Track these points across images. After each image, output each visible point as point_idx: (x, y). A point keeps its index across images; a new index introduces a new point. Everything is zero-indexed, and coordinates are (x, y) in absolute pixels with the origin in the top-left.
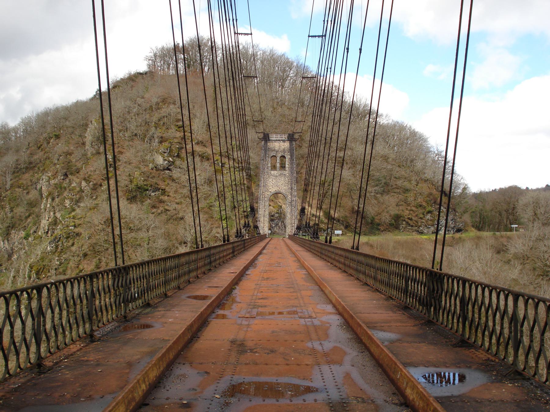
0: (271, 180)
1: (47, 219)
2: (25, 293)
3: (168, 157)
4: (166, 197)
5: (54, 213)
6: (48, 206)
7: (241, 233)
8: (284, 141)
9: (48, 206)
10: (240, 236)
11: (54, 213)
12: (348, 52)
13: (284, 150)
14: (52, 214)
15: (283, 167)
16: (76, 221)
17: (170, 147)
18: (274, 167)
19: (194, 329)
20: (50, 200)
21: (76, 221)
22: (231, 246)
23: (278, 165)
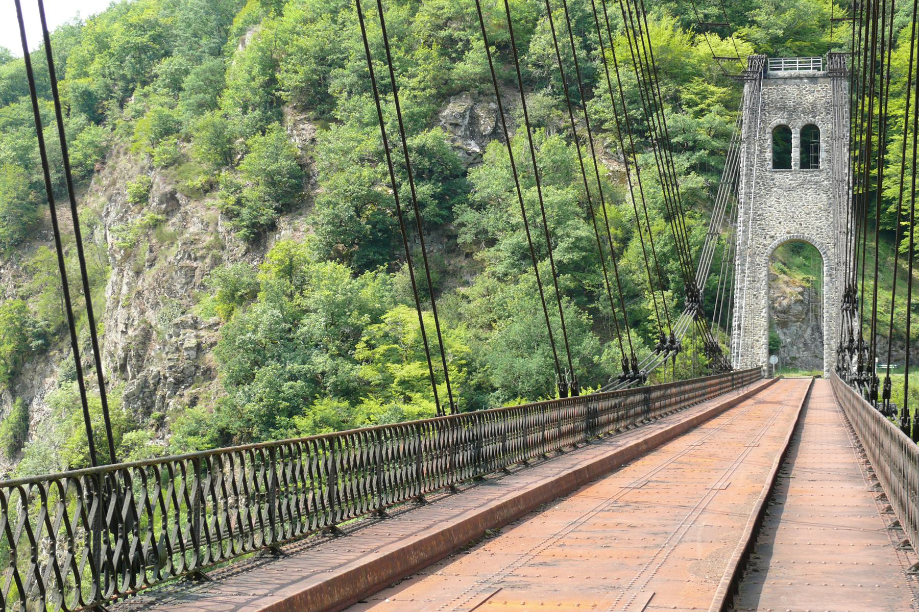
0: (772, 200)
1: (121, 327)
2: (36, 486)
3: (464, 138)
4: (462, 258)
5: (142, 312)
6: (125, 289)
7: (635, 368)
8: (813, 79)
9: (125, 289)
10: (632, 379)
11: (142, 312)
12: (7, 528)
13: (814, 105)
14: (135, 312)
15: (810, 160)
16: (202, 333)
17: (472, 108)
18: (781, 161)
19: (362, 585)
20: (129, 273)
21: (202, 333)
22: (579, 409)
23: (796, 154)
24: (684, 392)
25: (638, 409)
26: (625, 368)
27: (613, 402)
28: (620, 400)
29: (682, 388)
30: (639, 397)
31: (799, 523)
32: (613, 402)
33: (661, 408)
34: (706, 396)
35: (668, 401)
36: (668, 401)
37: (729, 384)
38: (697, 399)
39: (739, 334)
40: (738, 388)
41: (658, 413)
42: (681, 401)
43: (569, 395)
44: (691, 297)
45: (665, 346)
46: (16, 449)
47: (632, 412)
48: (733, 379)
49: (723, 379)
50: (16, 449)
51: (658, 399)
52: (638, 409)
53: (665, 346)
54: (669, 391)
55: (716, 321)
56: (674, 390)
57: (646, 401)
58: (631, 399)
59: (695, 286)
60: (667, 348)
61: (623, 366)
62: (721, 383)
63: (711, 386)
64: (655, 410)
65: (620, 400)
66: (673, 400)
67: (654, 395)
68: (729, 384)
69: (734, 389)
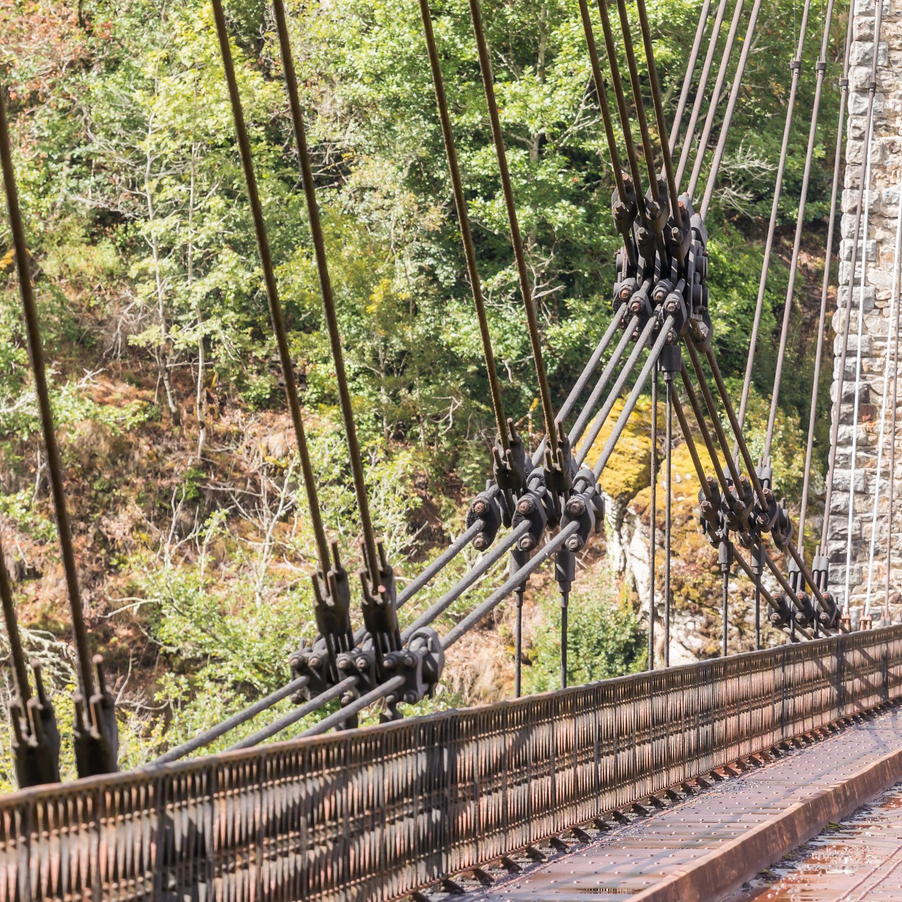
7: (380, 619)
24: (617, 739)
25: (400, 832)
26: (332, 621)
27: (282, 796)
28: (314, 785)
29: (607, 717)
30: (405, 768)
31: (668, 748)
32: (282, 796)
33: (504, 823)
34: (719, 758)
35: (540, 787)
36: (540, 787)
37: (826, 693)
38: (676, 775)
39: (866, 446)
40: (868, 715)
41: (491, 847)
42: (600, 787)
43: (69, 775)
44: (648, 244)
45: (521, 503)
46: (519, 696)
47: (368, 844)
48: (842, 671)
49: (796, 671)
50: (519, 696)
51: (493, 774)
52: (400, 832)
53: (521, 503)
54: (541, 735)
55: (762, 387)
56: (566, 729)
57: (437, 788)
58: (370, 781)
59: (665, 191)
60: (531, 514)
61: (322, 610)
62: (785, 689)
63: (739, 703)
64: (475, 834)
65: (314, 785)
66: (565, 778)
67: (475, 755)
68: (826, 693)
69: (844, 723)
